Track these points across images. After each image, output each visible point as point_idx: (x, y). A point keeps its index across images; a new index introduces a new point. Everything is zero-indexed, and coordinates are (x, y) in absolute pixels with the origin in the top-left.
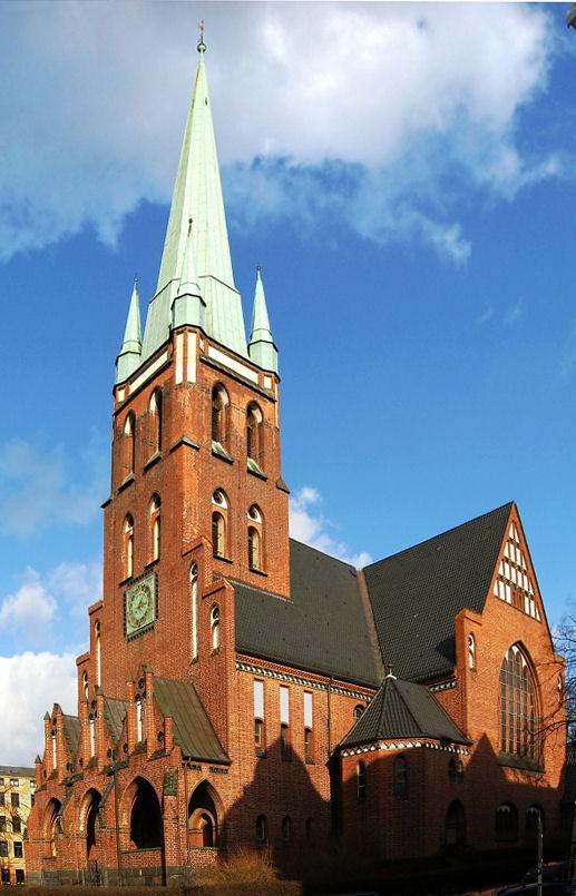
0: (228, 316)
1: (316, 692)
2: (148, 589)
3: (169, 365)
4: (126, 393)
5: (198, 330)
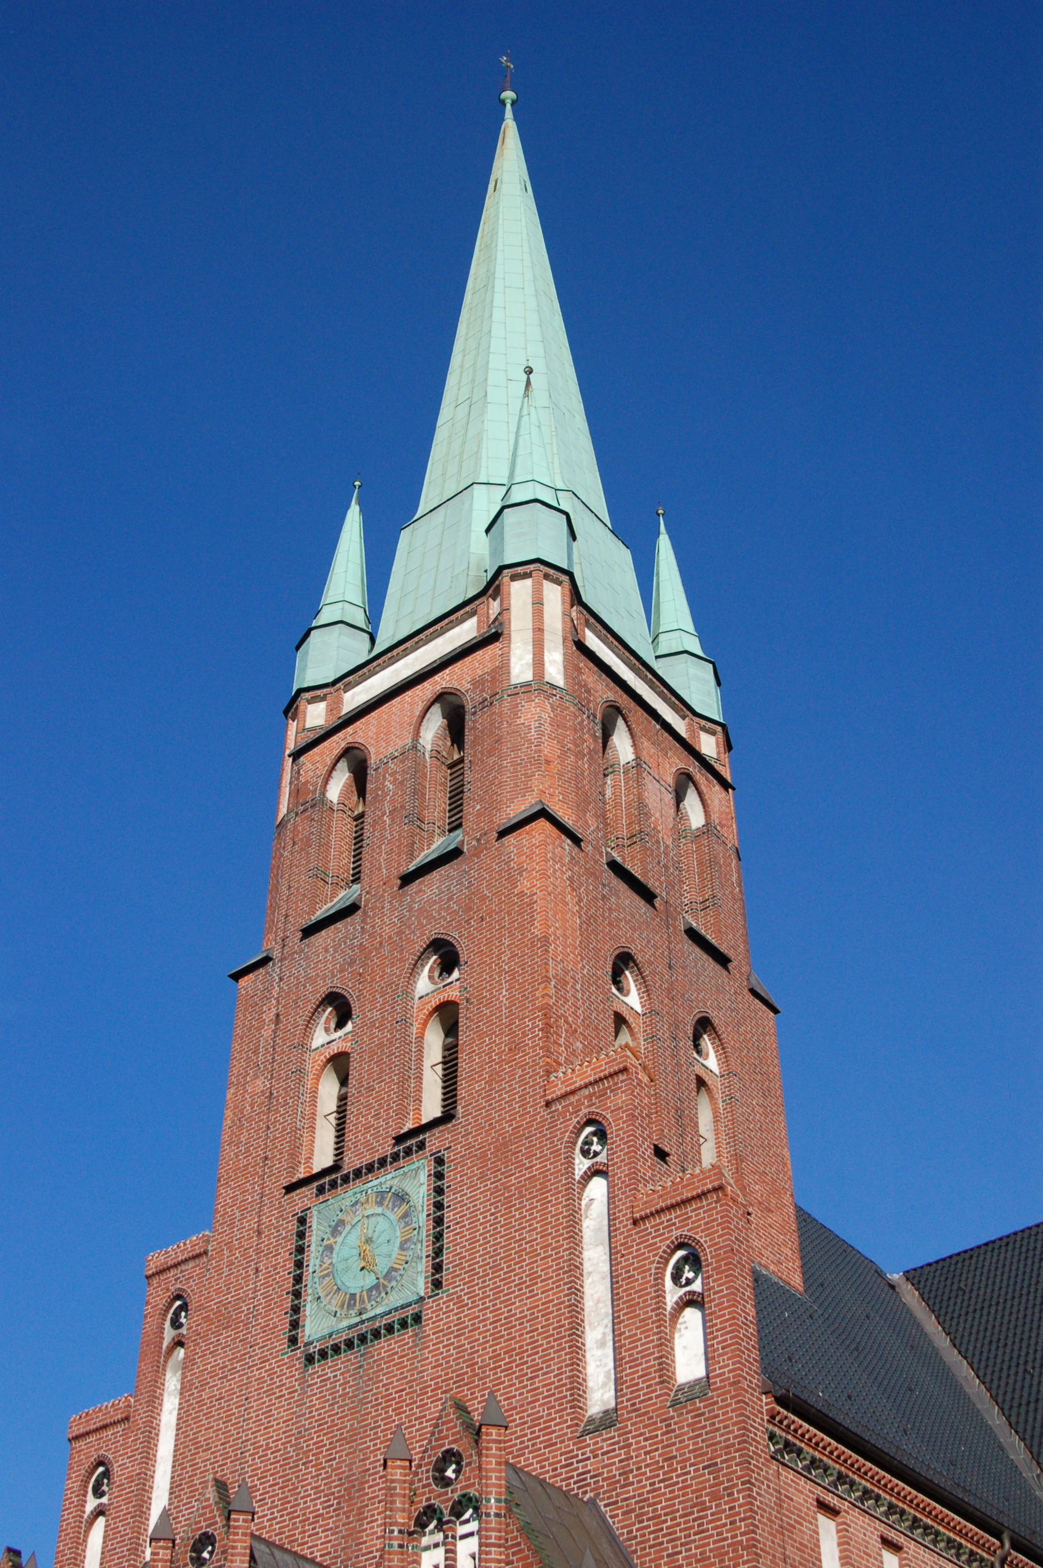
0: (1029, 1368)
1: (910, 1547)
2: (401, 1198)
3: (493, 637)
4: (330, 710)
5: (565, 578)
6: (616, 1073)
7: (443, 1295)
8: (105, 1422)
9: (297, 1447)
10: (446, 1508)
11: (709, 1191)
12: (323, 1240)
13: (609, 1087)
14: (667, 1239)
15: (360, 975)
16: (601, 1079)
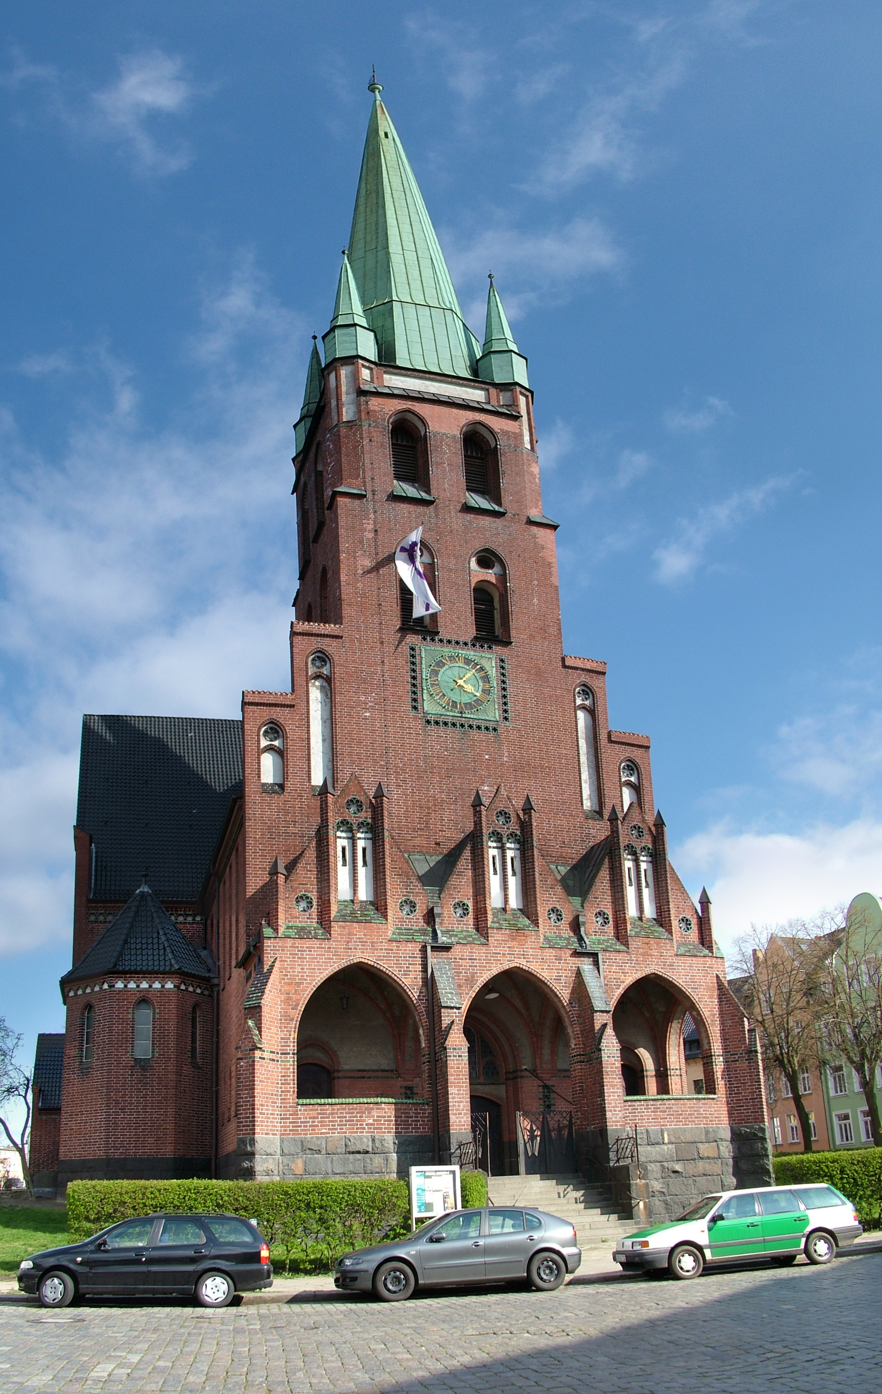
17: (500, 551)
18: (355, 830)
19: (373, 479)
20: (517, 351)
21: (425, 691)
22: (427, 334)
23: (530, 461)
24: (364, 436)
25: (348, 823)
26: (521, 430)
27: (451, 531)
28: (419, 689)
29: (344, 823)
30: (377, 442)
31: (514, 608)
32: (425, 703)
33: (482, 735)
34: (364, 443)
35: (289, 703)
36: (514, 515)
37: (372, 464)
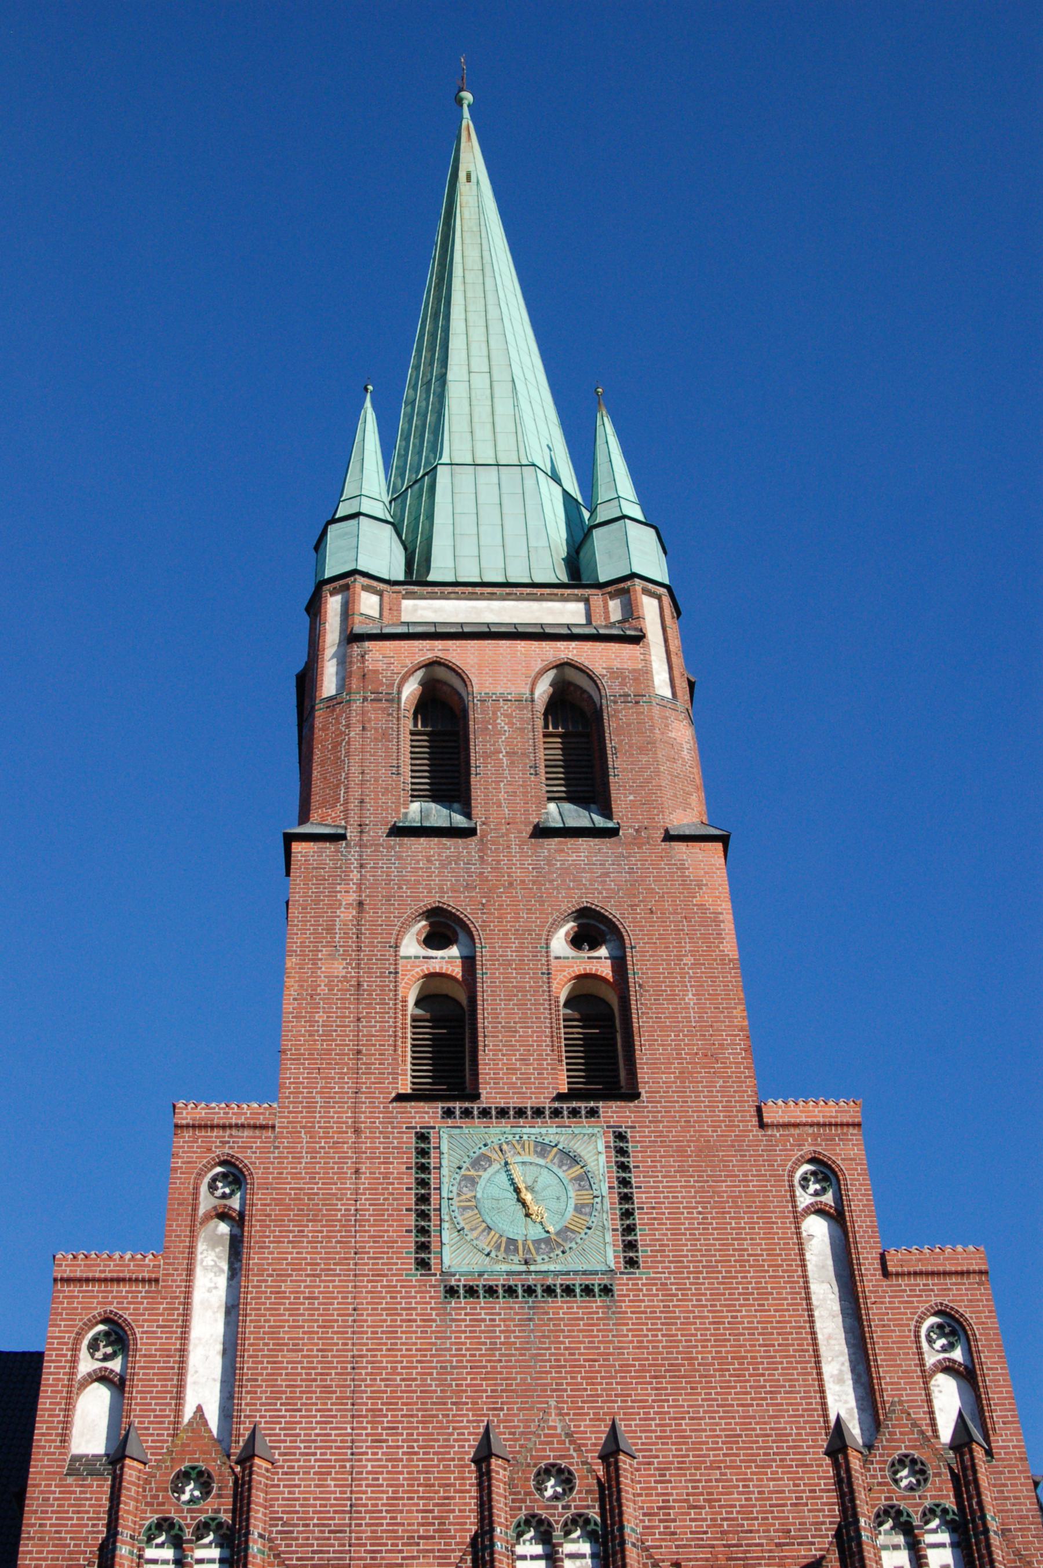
6: (848, 1125)
7: (641, 1275)
8: (121, 1275)
9: (441, 1382)
10: (916, 1513)
11: (974, 1272)
12: (460, 1168)
13: (838, 1135)
14: (926, 1302)
15: (483, 905)
16: (830, 1125)
17: (612, 911)
18: (190, 1541)
19: (362, 802)
20: (641, 518)
21: (445, 1225)
22: (490, 516)
23: (667, 718)
24: (354, 720)
25: (172, 1525)
26: (647, 662)
27: (511, 884)
28: (434, 1220)
29: (164, 1525)
30: (376, 729)
31: (643, 1021)
32: (446, 1250)
33: (578, 1305)
34: (352, 734)
35: (147, 1275)
36: (637, 831)
37: (363, 773)
